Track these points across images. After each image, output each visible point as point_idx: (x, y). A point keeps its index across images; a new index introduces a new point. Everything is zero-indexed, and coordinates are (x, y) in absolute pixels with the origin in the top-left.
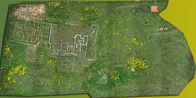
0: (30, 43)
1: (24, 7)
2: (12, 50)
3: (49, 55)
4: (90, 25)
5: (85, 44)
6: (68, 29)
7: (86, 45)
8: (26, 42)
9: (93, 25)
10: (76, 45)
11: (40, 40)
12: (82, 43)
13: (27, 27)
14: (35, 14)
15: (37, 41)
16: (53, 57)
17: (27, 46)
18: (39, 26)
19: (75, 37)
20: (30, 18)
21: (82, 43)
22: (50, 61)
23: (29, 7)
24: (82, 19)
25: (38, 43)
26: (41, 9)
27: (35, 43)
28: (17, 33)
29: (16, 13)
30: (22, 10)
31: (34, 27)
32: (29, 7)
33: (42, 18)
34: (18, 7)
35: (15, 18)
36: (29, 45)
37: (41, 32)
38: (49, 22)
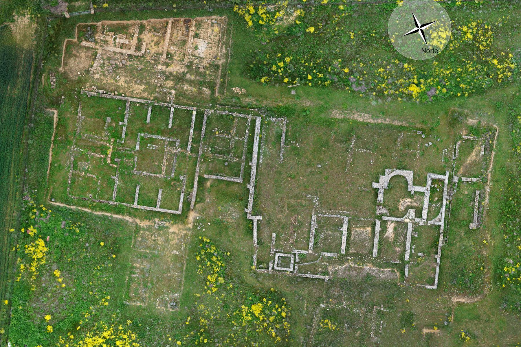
0: (151, 215)
1: (118, 30)
2: (59, 255)
3: (249, 279)
4: (455, 121)
5: (433, 214)
6: (347, 141)
7: (440, 220)
8: (133, 212)
9: (472, 121)
10: (384, 224)
11: (200, 199)
12: (419, 214)
13: (132, 134)
14: (176, 68)
15: (187, 203)
16: (269, 285)
17: (138, 229)
18: (198, 128)
19: (384, 180)
20: (151, 88)
21: (419, 214)
22: (257, 309)
23: (142, 28)
24: (414, 89)
25: (192, 216)
26: (205, 42)
27: (174, 217)
28: (84, 165)
29: (76, 65)
30: (111, 48)
31: (170, 133)
32: (142, 28)
33: (212, 88)
34: (89, 33)
35: (72, 90)
36: (145, 224)
37: (205, 158)
38: (243, 109)
